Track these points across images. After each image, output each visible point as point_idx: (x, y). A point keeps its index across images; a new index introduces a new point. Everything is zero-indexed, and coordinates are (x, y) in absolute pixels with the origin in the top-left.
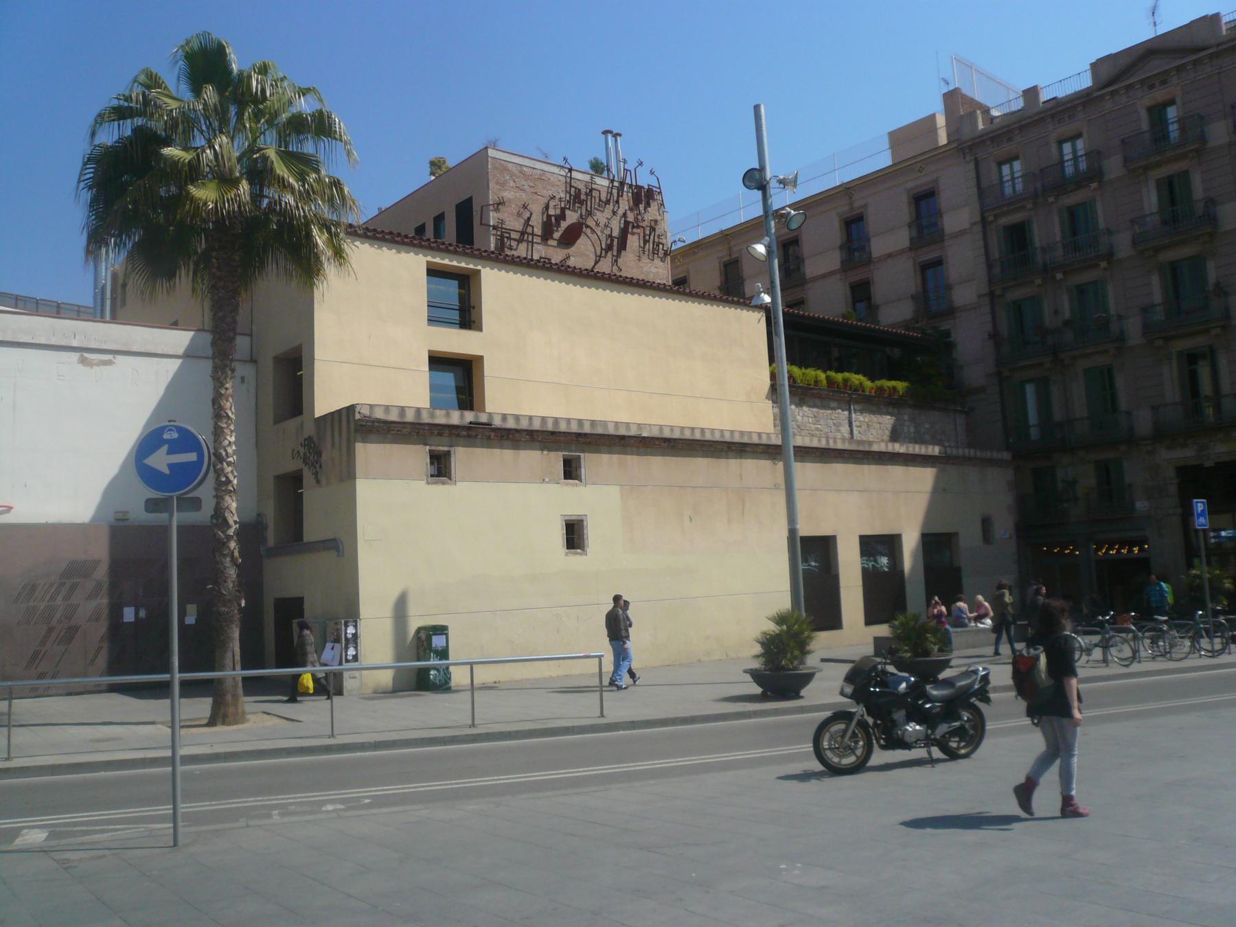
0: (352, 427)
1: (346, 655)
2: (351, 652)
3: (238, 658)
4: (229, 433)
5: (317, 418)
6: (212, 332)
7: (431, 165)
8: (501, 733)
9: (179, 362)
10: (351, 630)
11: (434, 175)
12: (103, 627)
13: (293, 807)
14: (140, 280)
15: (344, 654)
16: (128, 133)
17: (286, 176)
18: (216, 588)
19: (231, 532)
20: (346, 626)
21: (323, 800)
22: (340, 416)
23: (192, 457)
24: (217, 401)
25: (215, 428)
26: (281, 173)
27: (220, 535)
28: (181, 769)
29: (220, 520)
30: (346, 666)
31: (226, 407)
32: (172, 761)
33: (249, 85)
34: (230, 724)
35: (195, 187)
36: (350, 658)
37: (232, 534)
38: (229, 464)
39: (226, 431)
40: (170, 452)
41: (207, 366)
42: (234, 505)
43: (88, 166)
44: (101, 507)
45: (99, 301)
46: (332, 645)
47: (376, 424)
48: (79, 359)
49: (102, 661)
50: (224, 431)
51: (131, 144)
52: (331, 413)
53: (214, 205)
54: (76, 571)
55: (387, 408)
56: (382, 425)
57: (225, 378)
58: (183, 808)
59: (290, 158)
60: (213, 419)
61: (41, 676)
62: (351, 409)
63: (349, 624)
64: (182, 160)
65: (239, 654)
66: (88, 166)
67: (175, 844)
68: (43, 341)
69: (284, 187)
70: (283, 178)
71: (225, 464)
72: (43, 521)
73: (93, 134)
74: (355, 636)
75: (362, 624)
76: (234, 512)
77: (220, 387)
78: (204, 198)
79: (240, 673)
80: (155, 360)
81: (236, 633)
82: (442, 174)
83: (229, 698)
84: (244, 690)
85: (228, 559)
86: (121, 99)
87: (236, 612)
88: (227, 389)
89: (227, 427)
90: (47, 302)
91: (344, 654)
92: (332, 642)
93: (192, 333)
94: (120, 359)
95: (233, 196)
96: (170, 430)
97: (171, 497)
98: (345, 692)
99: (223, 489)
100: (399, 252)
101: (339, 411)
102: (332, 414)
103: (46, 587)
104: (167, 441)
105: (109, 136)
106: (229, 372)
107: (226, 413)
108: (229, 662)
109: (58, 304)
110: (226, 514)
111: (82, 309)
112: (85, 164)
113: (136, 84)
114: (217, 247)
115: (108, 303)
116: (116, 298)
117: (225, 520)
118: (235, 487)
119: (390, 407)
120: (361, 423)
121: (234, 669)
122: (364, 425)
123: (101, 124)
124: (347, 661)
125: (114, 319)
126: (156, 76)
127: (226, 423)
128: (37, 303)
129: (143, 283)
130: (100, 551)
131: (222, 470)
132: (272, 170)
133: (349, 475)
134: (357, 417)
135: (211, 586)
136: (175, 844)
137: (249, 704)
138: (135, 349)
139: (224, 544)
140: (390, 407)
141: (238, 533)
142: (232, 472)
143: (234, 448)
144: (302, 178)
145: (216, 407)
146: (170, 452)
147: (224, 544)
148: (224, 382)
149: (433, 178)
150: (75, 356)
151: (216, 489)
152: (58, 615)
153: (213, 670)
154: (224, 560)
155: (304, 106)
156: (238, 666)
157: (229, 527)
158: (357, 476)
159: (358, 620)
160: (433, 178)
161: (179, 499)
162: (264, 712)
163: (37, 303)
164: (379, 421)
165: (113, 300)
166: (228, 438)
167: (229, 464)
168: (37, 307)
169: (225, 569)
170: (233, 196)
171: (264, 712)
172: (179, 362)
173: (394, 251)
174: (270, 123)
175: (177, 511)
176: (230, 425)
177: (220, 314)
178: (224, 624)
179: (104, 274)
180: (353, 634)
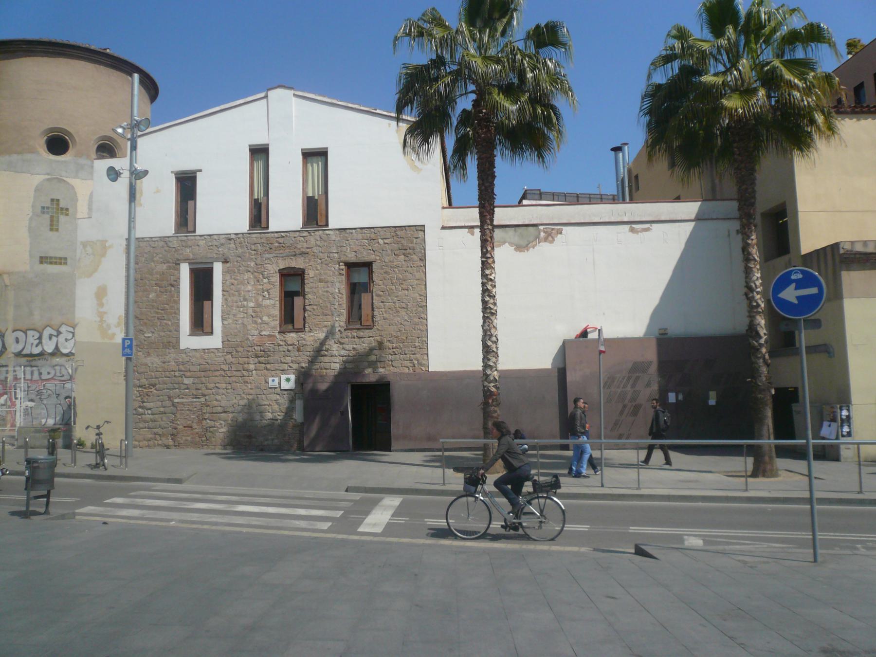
1: (842, 431)
2: (846, 429)
3: (771, 430)
4: (757, 271)
5: (803, 255)
6: (738, 200)
7: (848, 47)
8: (585, 494)
9: (693, 224)
10: (845, 413)
11: (851, 54)
13: (871, 544)
14: (680, 172)
15: (840, 430)
16: (676, 71)
17: (792, 79)
18: (754, 381)
19: (762, 341)
20: (841, 409)
21: (865, 540)
22: (825, 255)
23: (814, 291)
24: (745, 249)
25: (745, 268)
27: (754, 344)
28: (817, 507)
29: (754, 333)
30: (843, 440)
32: (810, 501)
33: (759, 17)
34: (768, 477)
36: (845, 434)
37: (763, 343)
38: (758, 293)
39: (754, 269)
40: (796, 288)
41: (736, 225)
42: (763, 322)
43: (645, 100)
44: (650, 326)
47: (858, 256)
48: (629, 229)
50: (752, 270)
51: (679, 78)
52: (823, 248)
53: (743, 110)
54: (638, 368)
55: (865, 243)
56: (863, 256)
57: (751, 232)
58: (820, 535)
59: (792, 65)
60: (743, 262)
61: (620, 437)
62: (835, 247)
63: (843, 408)
65: (772, 428)
66: (645, 100)
67: (815, 561)
68: (607, 220)
70: (790, 81)
71: (755, 293)
72: (615, 336)
73: (649, 76)
74: (848, 417)
75: (853, 408)
76: (763, 326)
78: (734, 106)
80: (677, 224)
81: (769, 413)
82: (858, 52)
83: (767, 458)
84: (776, 454)
85: (761, 360)
86: (668, 50)
87: (769, 397)
88: (752, 240)
90: (572, 195)
91: (840, 430)
92: (828, 421)
93: (699, 203)
94: (654, 226)
95: (755, 101)
96: (795, 273)
97: (800, 319)
99: (755, 310)
100: (859, 120)
101: (824, 249)
102: (817, 251)
103: (620, 379)
104: (795, 281)
105: (660, 78)
106: (753, 228)
107: (754, 257)
108: (765, 432)
109: (577, 195)
110: (758, 329)
111: (591, 196)
112: (643, 99)
113: (668, 37)
114: (737, 139)
116: (631, 186)
117: (758, 334)
118: (763, 309)
119: (868, 242)
120: (845, 256)
121: (769, 439)
122: (848, 258)
123: (655, 69)
124: (843, 436)
125: (632, 200)
127: (754, 264)
128: (553, 195)
129: (682, 173)
130: (651, 355)
131: (753, 297)
132: (781, 76)
133: (837, 295)
134: (842, 251)
135: (750, 380)
136: (815, 561)
137: (782, 463)
138: (663, 218)
139: (758, 350)
140: (868, 242)
141: (766, 341)
142: (760, 299)
143: (760, 281)
144: (802, 77)
145: (746, 253)
146: (796, 288)
147: (758, 350)
148: (750, 235)
149: (850, 56)
151: (749, 312)
152: (629, 397)
153: (794, 439)
154: (758, 361)
155: (797, 23)
156: (772, 437)
157: (761, 337)
158: (844, 296)
159: (850, 405)
160: (850, 56)
161: (805, 320)
162: (786, 470)
163: (553, 195)
165: (630, 187)
166: (756, 274)
167: (758, 293)
168: (553, 197)
169: (760, 368)
170: (755, 101)
171: (786, 470)
172: (693, 224)
173: (855, 120)
174: (767, 42)
175: (805, 329)
176: (756, 265)
177: (744, 187)
178: (761, 406)
179: (622, 171)
180: (846, 416)
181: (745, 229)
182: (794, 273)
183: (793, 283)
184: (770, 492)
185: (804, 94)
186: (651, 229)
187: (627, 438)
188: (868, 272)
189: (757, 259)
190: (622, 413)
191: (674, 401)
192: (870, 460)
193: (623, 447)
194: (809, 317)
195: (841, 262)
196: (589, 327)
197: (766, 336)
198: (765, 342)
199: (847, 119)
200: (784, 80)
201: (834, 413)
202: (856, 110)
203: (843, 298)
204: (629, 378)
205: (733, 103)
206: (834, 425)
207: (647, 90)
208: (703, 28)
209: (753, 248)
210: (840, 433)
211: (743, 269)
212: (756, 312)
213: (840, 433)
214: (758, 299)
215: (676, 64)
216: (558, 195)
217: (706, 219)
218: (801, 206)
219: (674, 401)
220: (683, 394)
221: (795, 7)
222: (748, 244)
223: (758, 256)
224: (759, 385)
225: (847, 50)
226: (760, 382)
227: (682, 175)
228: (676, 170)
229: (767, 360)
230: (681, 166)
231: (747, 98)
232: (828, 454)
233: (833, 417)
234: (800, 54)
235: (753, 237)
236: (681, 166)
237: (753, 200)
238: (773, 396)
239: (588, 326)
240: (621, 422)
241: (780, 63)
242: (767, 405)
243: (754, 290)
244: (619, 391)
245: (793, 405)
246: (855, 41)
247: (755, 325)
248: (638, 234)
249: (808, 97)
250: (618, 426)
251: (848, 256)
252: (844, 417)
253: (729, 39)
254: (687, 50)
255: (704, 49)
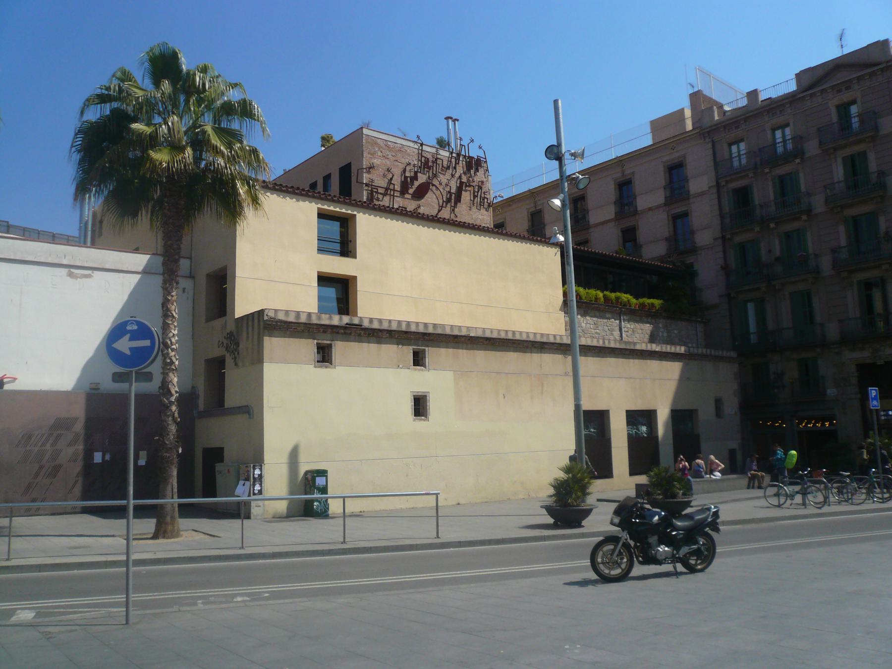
0: (262, 323)
1: (254, 490)
2: (257, 487)
3: (175, 490)
4: (174, 328)
9: (138, 276)
10: (257, 472)
11: (324, 147)
12: (78, 467)
13: (213, 598)
15: (252, 489)
17: (218, 145)
19: (173, 399)
20: (254, 469)
22: (248, 319)
23: (147, 343)
24: (165, 304)
26: (215, 143)
27: (165, 401)
28: (132, 569)
30: (253, 497)
31: (171, 309)
32: (126, 563)
33: (194, 80)
34: (168, 538)
35: (153, 151)
36: (256, 492)
37: (174, 400)
38: (173, 350)
39: (171, 326)
40: (131, 339)
42: (176, 380)
43: (78, 136)
44: (80, 380)
45: (83, 232)
46: (244, 482)
49: (78, 490)
50: (169, 327)
53: (167, 165)
54: (61, 425)
57: (172, 288)
58: (134, 597)
59: (221, 132)
62: (261, 313)
64: (145, 132)
66: (78, 136)
67: (127, 623)
68: (43, 260)
69: (217, 152)
70: (217, 146)
71: (170, 350)
72: (38, 389)
74: (260, 476)
75: (265, 468)
76: (176, 384)
77: (168, 295)
78: (160, 159)
79: (177, 500)
80: (122, 274)
83: (168, 519)
85: (170, 418)
86: (103, 89)
88: (172, 296)
89: (172, 324)
91: (252, 489)
92: (243, 480)
93: (149, 256)
94: (97, 274)
95: (180, 159)
97: (131, 372)
98: (252, 517)
100: (298, 201)
101: (253, 314)
104: (130, 331)
105: (93, 115)
106: (175, 284)
107: (172, 314)
109: (39, 231)
110: (170, 386)
112: (76, 134)
113: (114, 78)
114: (168, 194)
115: (89, 233)
117: (169, 391)
121: (172, 498)
124: (254, 494)
125: (94, 245)
126: (128, 73)
127: (171, 320)
128: (39, 233)
130: (79, 411)
131: (168, 354)
132: (209, 140)
133: (258, 360)
134: (266, 318)
135: (157, 438)
136: (127, 623)
137: (184, 523)
138: (107, 267)
139: (167, 408)
140: (289, 312)
141: (177, 400)
142: (175, 356)
143: (177, 338)
144: (230, 146)
145: (164, 309)
146: (131, 339)
147: (168, 407)
149: (323, 149)
150: (64, 271)
151: (163, 368)
152: (47, 457)
153: (215, 497)
154: (167, 419)
155: (234, 96)
156: (176, 496)
157: (172, 395)
159: (263, 465)
160: (323, 149)
161: (136, 373)
162: (193, 530)
163: (39, 233)
164: (281, 321)
165: (93, 231)
167: (173, 350)
170: (180, 159)
172: (138, 276)
173: (294, 200)
175: (135, 382)
176: (174, 322)
177: (169, 242)
181: (166, 285)
182: (130, 324)
183: (128, 333)
184: (155, 553)
185: (228, 162)
186: (93, 276)
187: (43, 501)
188: (287, 339)
189: (176, 316)
190: (37, 475)
191: (100, 461)
192: (278, 516)
193: (37, 513)
194: (141, 369)
195: (265, 328)
196: (6, 376)
197: (178, 394)
198: (175, 399)
199: (545, 247)
200: (210, 144)
201: (248, 471)
202: (309, 194)
203: (263, 362)
204: (51, 435)
205: (161, 157)
206: (247, 483)
207: (81, 126)
208: (145, 77)
209: (173, 304)
210: (252, 492)
211: (161, 324)
212: (169, 369)
213: (252, 492)
214: (172, 356)
215: (107, 109)
216: (29, 231)
217: (153, 273)
218: (238, 273)
219: (100, 461)
220: (110, 454)
221: (237, 81)
222: (169, 300)
223: (176, 313)
224: (166, 444)
225: (321, 143)
226: (167, 441)
227: (114, 221)
228: (109, 216)
229: (176, 418)
230: (113, 210)
231: (174, 154)
232: (240, 512)
233: (247, 475)
234: (235, 125)
235: (174, 294)
236: (113, 210)
237: (177, 257)
238: (179, 455)
239: (5, 375)
240: (34, 485)
241: (212, 128)
242: (172, 464)
243: (170, 347)
244: (36, 450)
245: (216, 465)
246: (328, 137)
247: (167, 382)
248: (77, 280)
249: (231, 165)
250: (31, 490)
251: (270, 323)
252: (256, 476)
253: (163, 93)
254: (122, 95)
255: (137, 96)
